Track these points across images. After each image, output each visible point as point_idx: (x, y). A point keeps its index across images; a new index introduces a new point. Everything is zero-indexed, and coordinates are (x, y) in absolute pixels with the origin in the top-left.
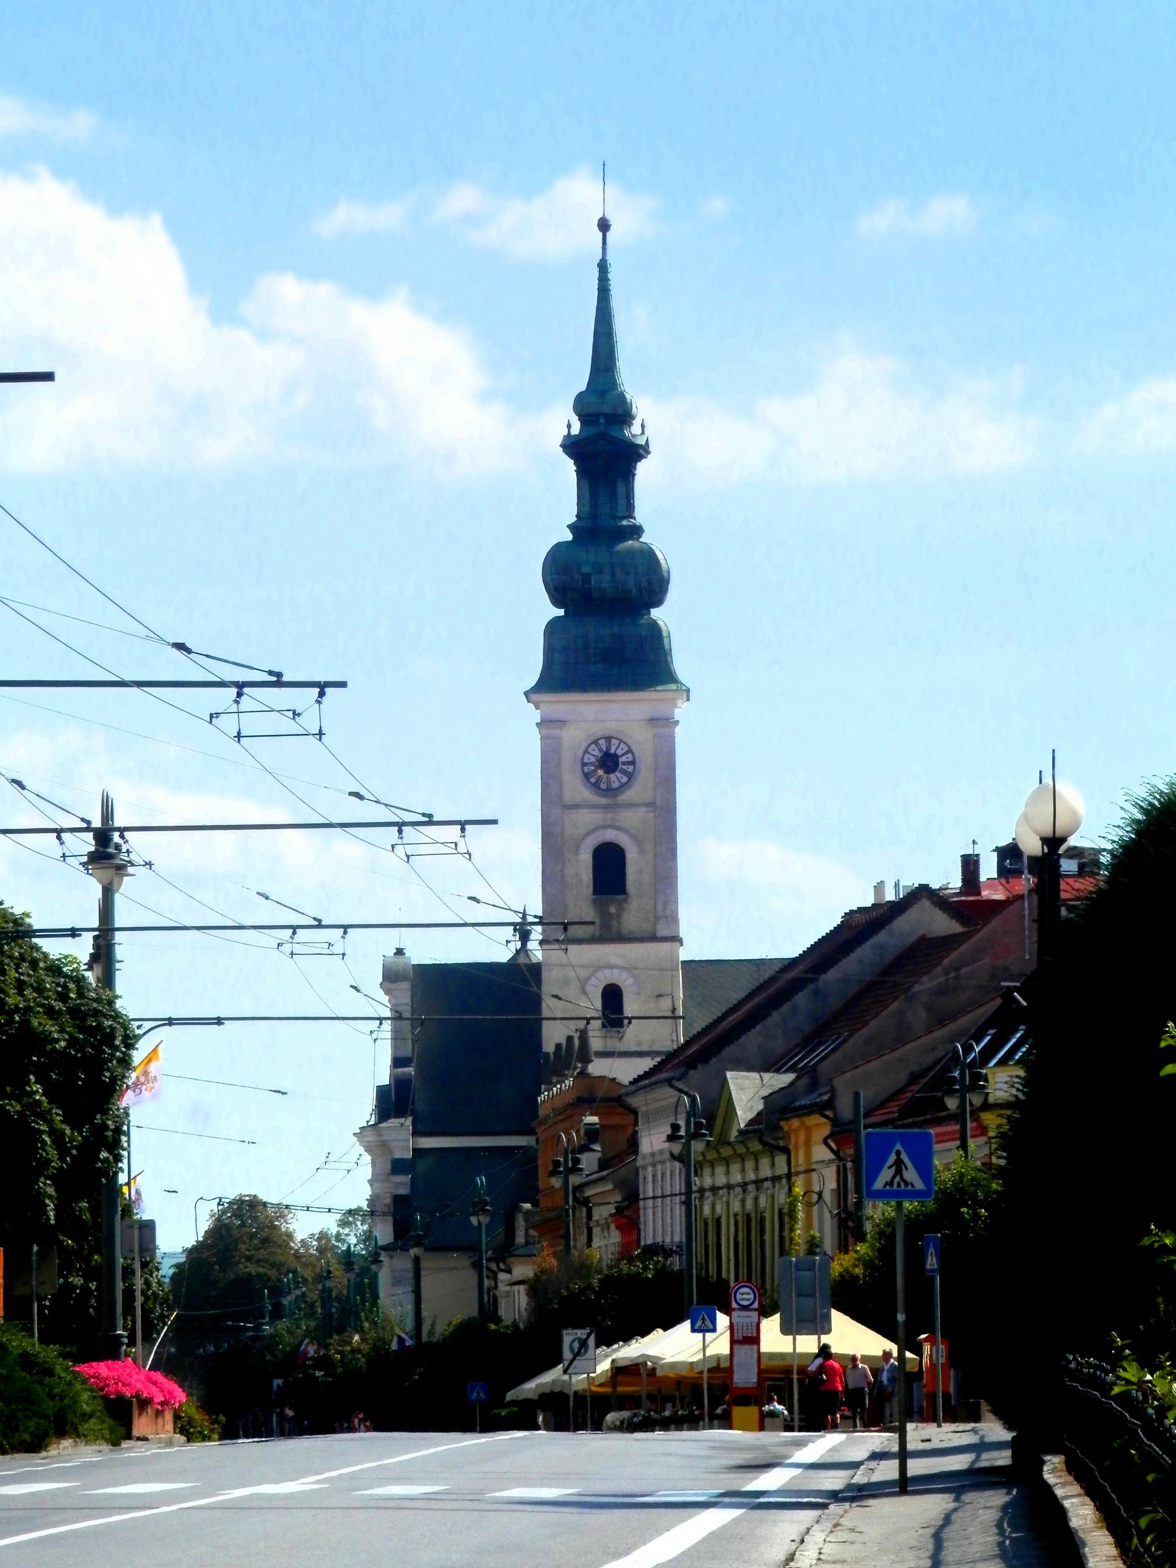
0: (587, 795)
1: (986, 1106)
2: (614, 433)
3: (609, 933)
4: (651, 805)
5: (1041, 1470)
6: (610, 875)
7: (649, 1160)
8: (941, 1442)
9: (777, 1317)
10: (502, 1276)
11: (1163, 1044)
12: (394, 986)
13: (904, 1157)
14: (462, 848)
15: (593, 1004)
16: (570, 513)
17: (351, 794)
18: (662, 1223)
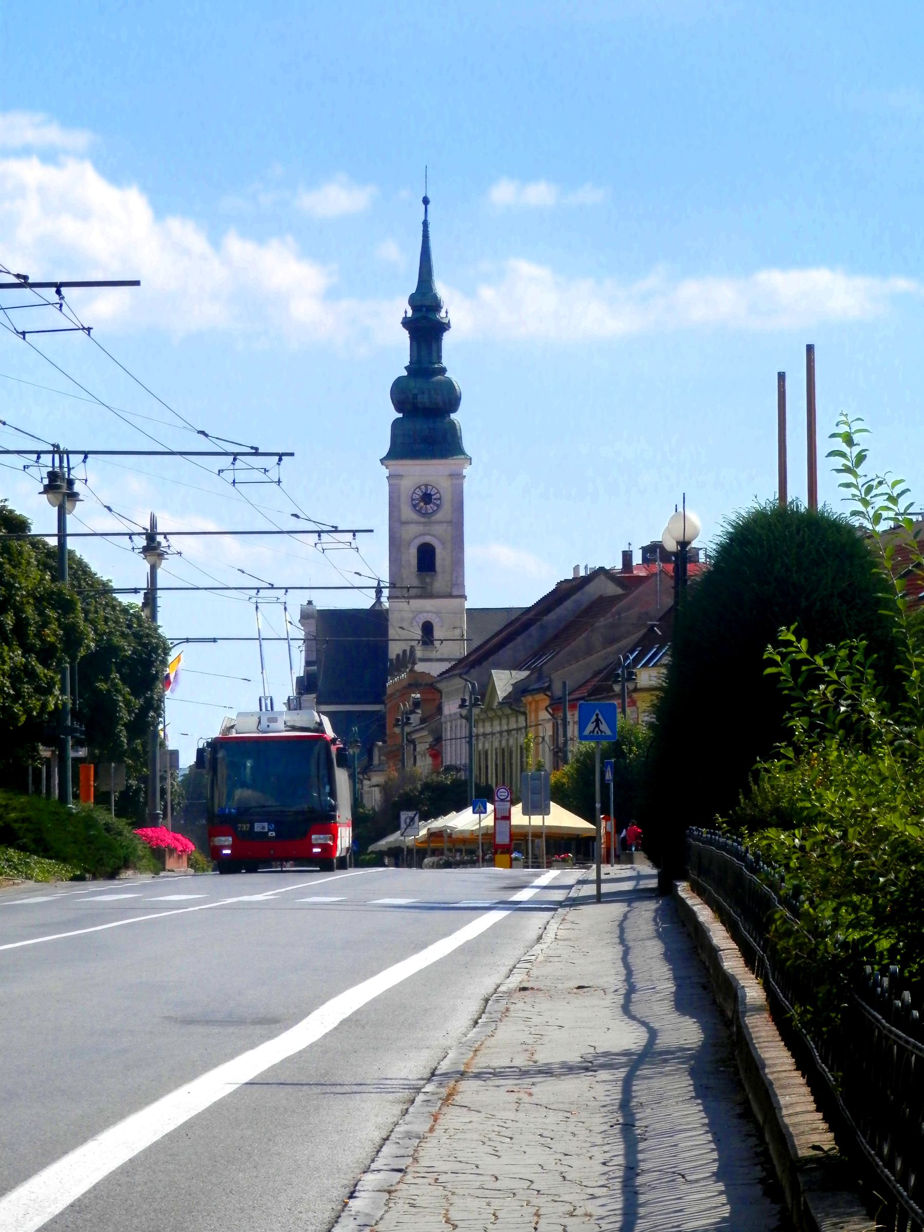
0: (414, 516)
1: (636, 690)
2: (431, 316)
3: (426, 593)
4: (450, 522)
5: (677, 890)
6: (427, 561)
7: (448, 718)
8: (618, 875)
9: (520, 806)
10: (366, 782)
11: (765, 657)
12: (307, 621)
13: (600, 717)
14: (353, 546)
15: (418, 633)
16: (407, 361)
17: (293, 515)
18: (455, 753)
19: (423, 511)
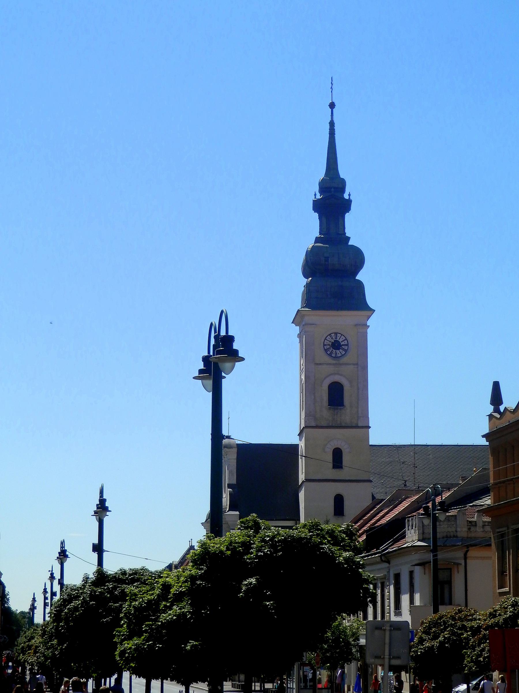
0: (326, 359)
6: (336, 395)
19: (333, 355)
